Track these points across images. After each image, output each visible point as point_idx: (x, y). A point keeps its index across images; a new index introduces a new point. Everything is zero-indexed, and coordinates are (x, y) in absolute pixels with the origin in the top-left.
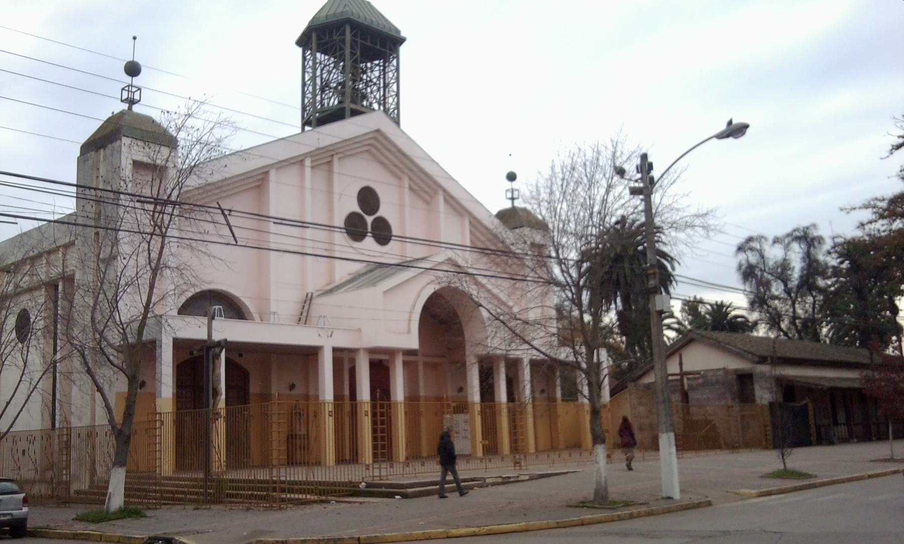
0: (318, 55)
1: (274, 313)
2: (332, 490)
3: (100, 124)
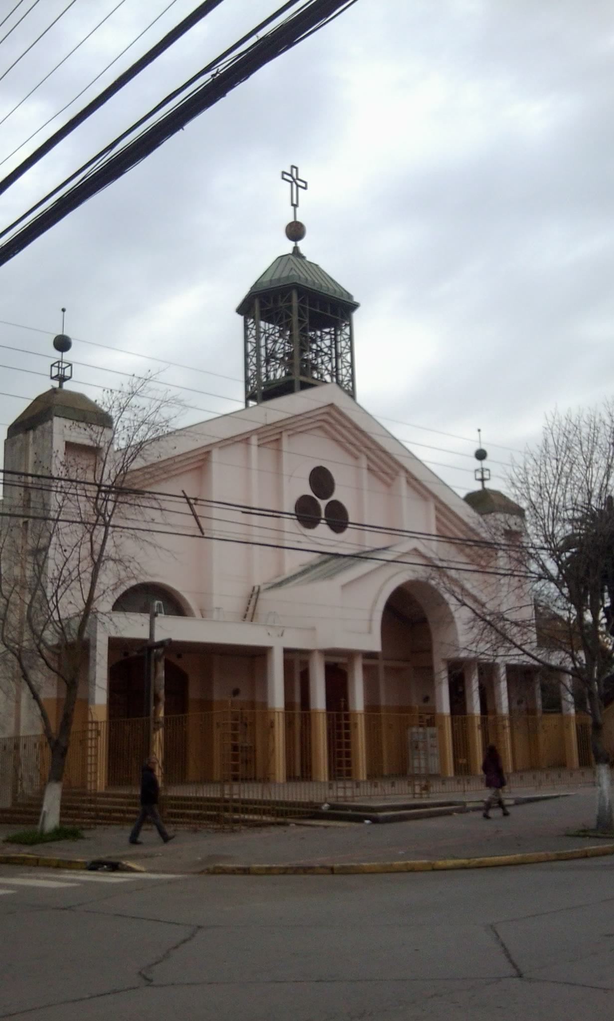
0: (262, 323)
1: (218, 609)
2: (290, 811)
3: (29, 402)
